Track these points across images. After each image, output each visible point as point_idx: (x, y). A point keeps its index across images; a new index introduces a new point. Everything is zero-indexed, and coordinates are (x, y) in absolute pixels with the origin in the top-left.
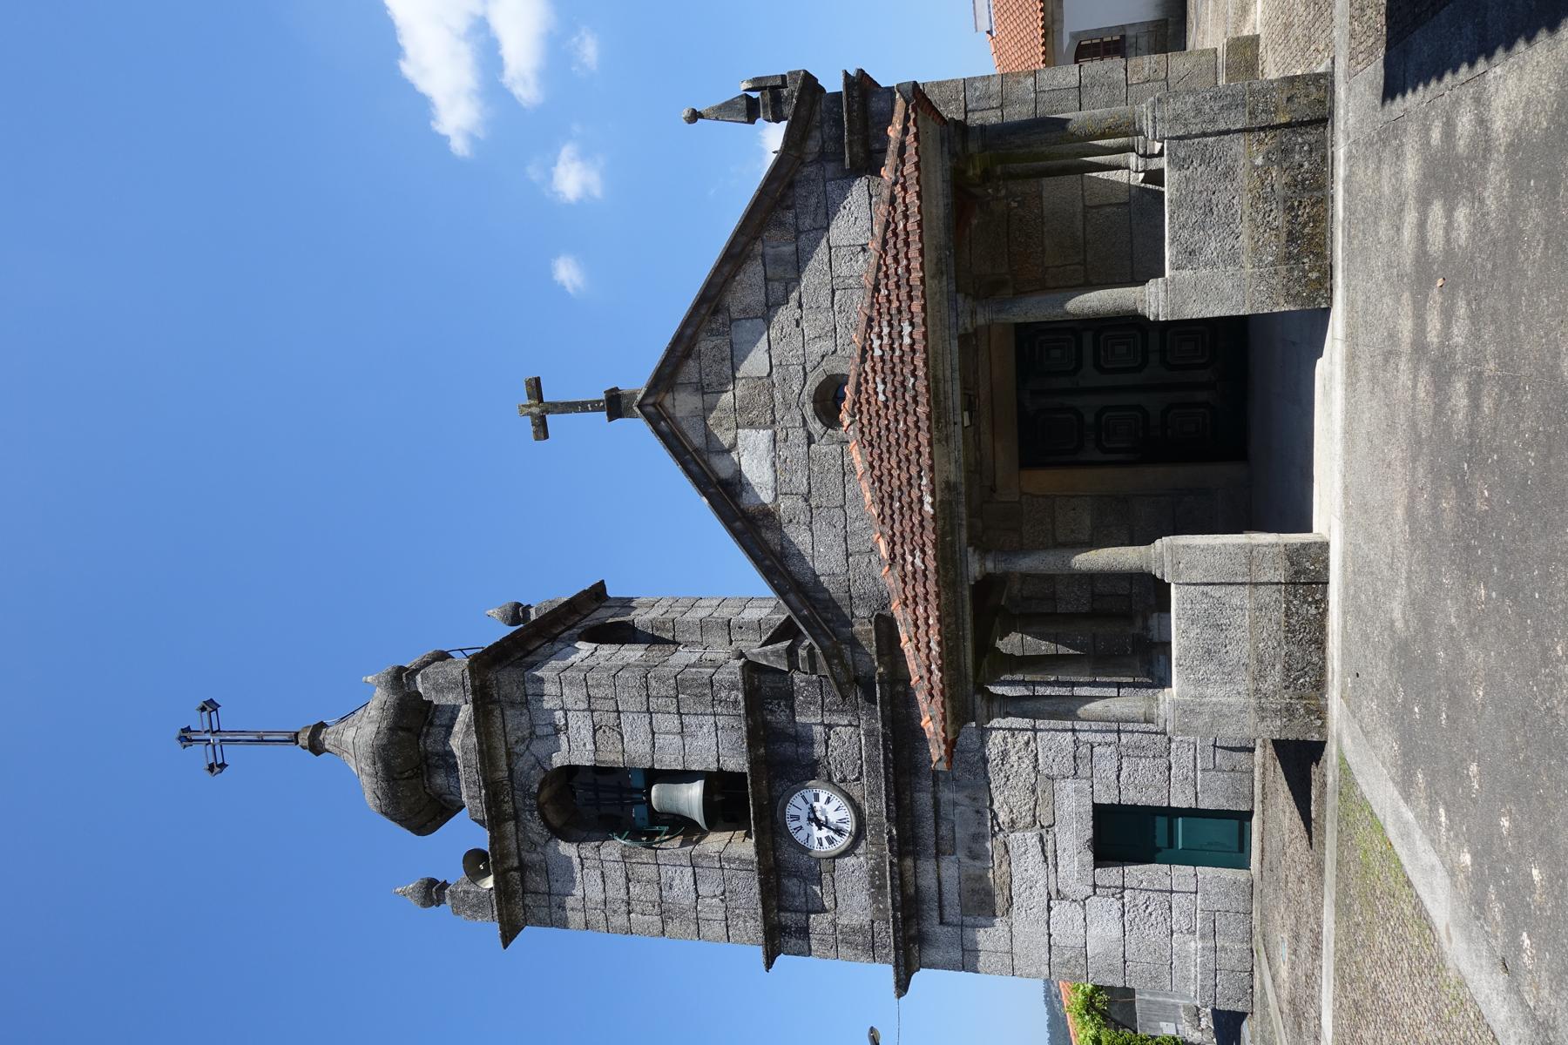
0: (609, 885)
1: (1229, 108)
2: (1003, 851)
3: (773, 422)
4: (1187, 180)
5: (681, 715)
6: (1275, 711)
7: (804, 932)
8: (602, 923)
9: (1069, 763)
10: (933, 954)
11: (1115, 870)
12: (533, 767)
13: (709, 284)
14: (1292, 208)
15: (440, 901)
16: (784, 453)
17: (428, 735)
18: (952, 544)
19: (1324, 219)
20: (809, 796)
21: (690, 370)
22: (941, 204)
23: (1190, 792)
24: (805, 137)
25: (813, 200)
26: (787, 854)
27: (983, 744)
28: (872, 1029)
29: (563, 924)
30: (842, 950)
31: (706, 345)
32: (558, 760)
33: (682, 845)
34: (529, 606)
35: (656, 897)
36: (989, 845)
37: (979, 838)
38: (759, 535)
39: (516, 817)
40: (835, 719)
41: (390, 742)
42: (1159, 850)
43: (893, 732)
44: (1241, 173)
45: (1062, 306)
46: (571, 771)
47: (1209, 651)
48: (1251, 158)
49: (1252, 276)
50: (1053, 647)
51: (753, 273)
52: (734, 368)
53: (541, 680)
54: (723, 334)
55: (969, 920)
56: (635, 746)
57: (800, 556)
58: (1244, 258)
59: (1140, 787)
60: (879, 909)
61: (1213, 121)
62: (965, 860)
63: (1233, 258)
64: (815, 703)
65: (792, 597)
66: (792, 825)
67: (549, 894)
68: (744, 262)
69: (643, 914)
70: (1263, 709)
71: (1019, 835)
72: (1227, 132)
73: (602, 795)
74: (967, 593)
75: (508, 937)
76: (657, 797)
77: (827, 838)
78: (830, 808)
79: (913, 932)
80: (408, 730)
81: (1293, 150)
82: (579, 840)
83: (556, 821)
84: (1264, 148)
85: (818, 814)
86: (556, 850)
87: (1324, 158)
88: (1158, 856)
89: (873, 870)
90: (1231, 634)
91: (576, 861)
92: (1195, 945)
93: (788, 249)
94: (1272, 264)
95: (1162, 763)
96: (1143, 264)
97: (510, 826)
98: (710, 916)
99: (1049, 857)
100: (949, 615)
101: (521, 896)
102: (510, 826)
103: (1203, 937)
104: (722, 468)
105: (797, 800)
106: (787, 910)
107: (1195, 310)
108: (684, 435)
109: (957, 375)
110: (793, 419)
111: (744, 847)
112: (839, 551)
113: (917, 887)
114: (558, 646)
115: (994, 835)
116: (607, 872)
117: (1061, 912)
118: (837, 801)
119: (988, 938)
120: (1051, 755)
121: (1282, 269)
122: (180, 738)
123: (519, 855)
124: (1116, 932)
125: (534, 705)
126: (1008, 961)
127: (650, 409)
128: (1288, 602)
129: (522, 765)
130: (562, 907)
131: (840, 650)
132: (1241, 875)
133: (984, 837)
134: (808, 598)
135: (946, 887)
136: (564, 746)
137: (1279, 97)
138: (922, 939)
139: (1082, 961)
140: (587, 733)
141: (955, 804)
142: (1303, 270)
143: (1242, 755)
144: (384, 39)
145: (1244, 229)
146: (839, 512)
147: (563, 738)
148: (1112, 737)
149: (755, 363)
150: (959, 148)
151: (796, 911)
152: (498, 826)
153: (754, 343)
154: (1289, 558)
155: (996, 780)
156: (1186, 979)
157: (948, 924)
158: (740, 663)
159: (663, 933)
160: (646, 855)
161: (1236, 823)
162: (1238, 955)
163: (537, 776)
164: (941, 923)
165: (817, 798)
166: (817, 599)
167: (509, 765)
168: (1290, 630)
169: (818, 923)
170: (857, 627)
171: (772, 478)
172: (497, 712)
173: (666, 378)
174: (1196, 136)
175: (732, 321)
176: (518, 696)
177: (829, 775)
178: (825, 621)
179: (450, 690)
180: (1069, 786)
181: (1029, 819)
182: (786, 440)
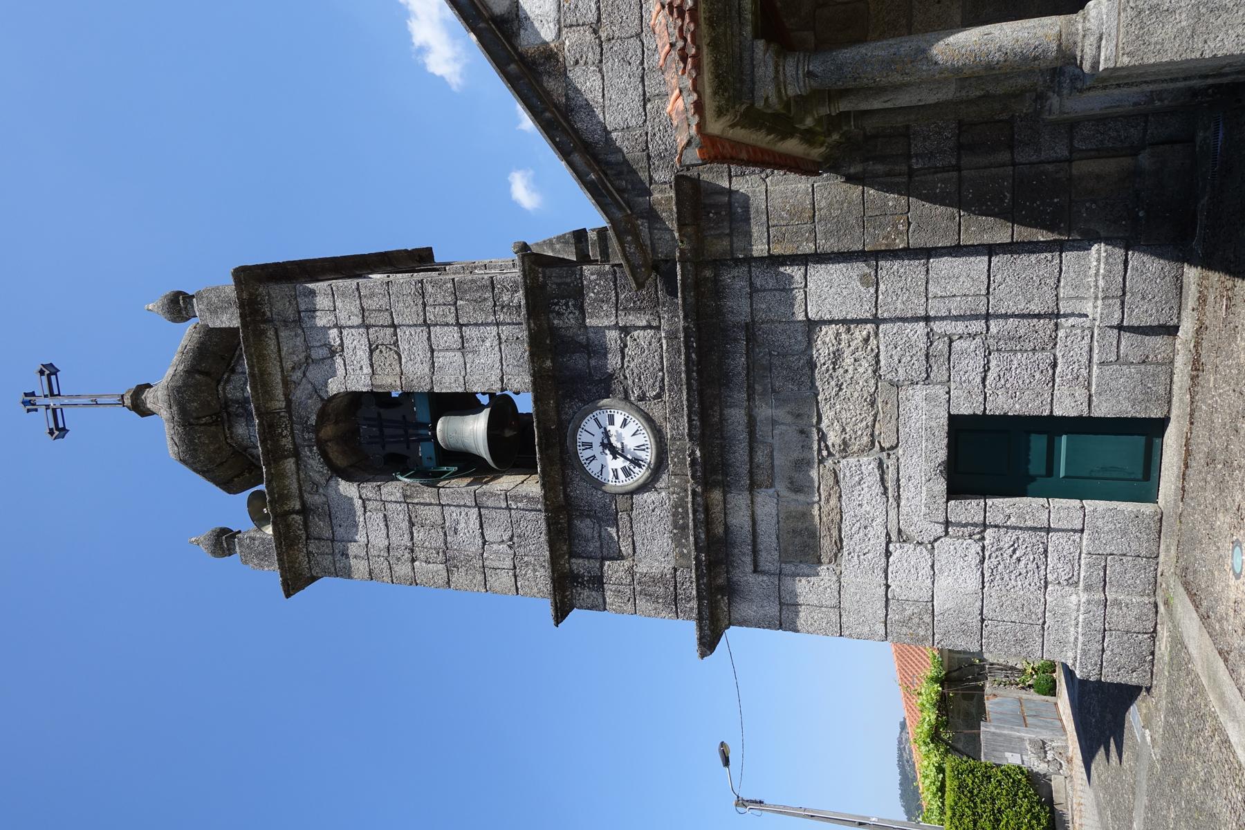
2: (831, 482)
5: (460, 326)
7: (598, 582)
8: (386, 572)
9: (920, 364)
10: (745, 609)
11: (974, 502)
15: (230, 552)
17: (228, 381)
23: (1081, 393)
26: (579, 490)
27: (810, 343)
28: (722, 744)
29: (347, 573)
30: (641, 603)
32: (334, 387)
35: (440, 543)
36: (814, 474)
37: (802, 465)
39: (296, 454)
40: (631, 319)
41: (185, 384)
42: (1033, 479)
43: (699, 329)
46: (355, 399)
55: (789, 568)
57: (588, 108)
59: (1010, 391)
60: (682, 555)
62: (784, 493)
64: (607, 302)
65: (576, 157)
66: (584, 454)
69: (428, 562)
71: (852, 460)
73: (387, 431)
76: (443, 431)
77: (624, 469)
78: (627, 433)
79: (721, 581)
80: (206, 374)
83: (340, 461)
85: (613, 440)
86: (337, 490)
88: (1031, 487)
89: (676, 507)
91: (358, 503)
92: (1077, 598)
95: (1045, 357)
97: (290, 464)
98: (496, 564)
99: (891, 490)
102: (290, 464)
103: (1088, 588)
105: (589, 424)
106: (580, 556)
111: (532, 486)
112: (635, 96)
113: (727, 527)
115: (821, 462)
116: (388, 513)
117: (905, 560)
118: (635, 423)
119: (809, 590)
120: (896, 354)
122: (24, 403)
123: (301, 497)
124: (973, 583)
125: (307, 323)
126: (834, 618)
129: (299, 394)
131: (635, 227)
132: (1147, 508)
133: (809, 464)
134: (598, 162)
135: (762, 527)
136: (341, 371)
138: (731, 590)
139: (927, 619)
140: (363, 354)
141: (774, 422)
143: (1158, 341)
144: (404, 14)
146: (635, 42)
147: (339, 360)
148: (978, 326)
151: (589, 558)
155: (825, 390)
156: (1062, 643)
157: (764, 573)
160: (428, 494)
161: (1140, 440)
162: (1136, 611)
163: (314, 406)
164: (755, 571)
165: (612, 422)
166: (608, 163)
167: (286, 396)
169: (614, 571)
170: (657, 195)
172: (271, 333)
176: (290, 313)
177: (626, 392)
178: (618, 190)
179: (224, 309)
180: (918, 394)
181: (866, 439)
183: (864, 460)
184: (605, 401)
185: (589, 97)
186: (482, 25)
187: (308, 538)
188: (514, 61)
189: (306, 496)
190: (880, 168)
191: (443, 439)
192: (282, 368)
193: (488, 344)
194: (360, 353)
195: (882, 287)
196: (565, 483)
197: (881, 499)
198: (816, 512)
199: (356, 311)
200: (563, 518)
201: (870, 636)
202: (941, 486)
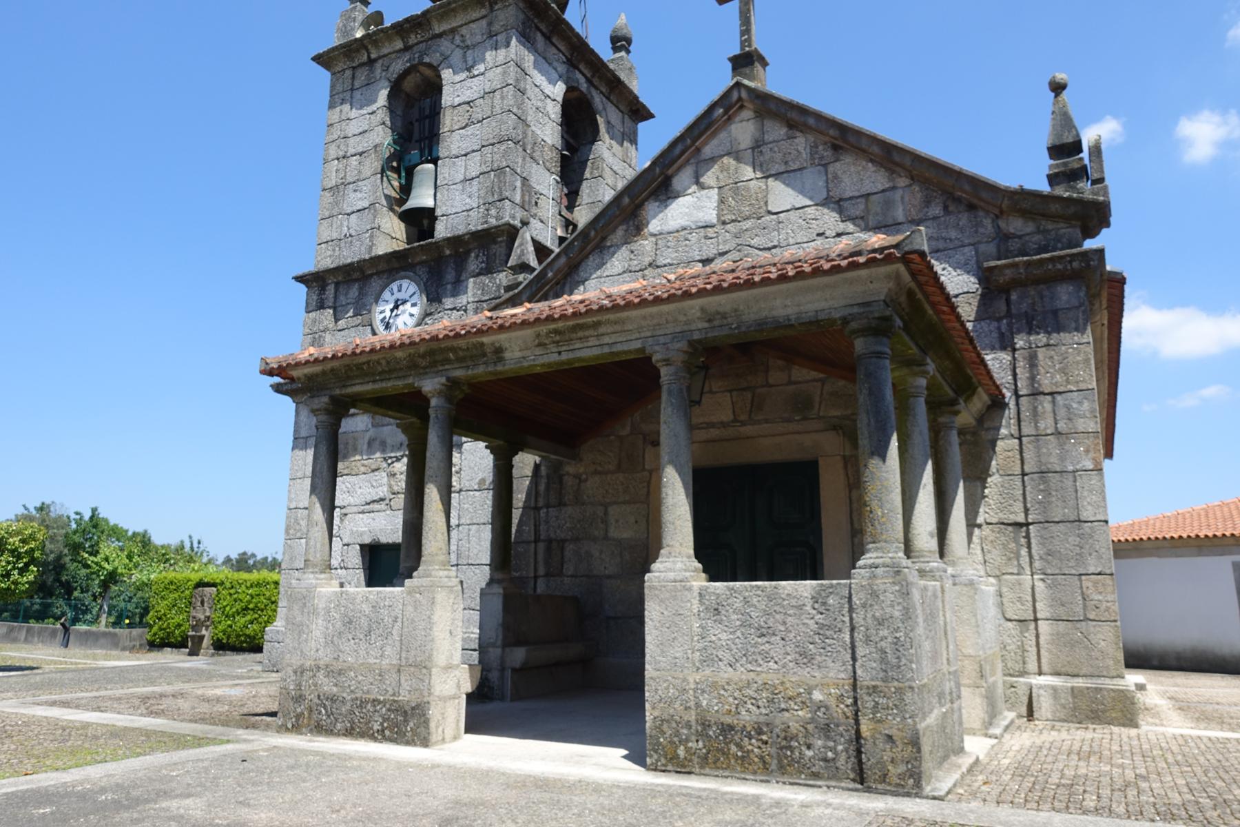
0: (358, 139)
1: (883, 660)
2: (374, 467)
3: (724, 223)
4: (800, 607)
6: (300, 685)
7: (321, 306)
12: (442, 55)
13: (859, 133)
14: (760, 732)
16: (694, 237)
18: (448, 361)
19: (745, 770)
20: (415, 299)
21: (776, 131)
22: (789, 311)
24: (1026, 214)
25: (953, 234)
26: (375, 283)
31: (801, 143)
33: (386, 196)
34: (628, 52)
35: (349, 179)
36: (378, 455)
38: (621, 223)
39: (407, 48)
44: (804, 673)
45: (671, 462)
47: (350, 622)
48: (823, 686)
49: (685, 680)
50: (521, 505)
51: (872, 179)
52: (777, 176)
53: (508, 45)
54: (812, 158)
56: (456, 138)
57: (601, 265)
58: (708, 672)
61: (868, 640)
63: (709, 660)
64: (482, 294)
66: (394, 286)
67: (352, 90)
68: (887, 169)
69: (337, 171)
70: (302, 673)
71: (386, 479)
72: (854, 659)
74: (410, 380)
75: (321, 59)
81: (828, 738)
82: (391, 108)
84: (832, 702)
87: (816, 776)
90: (363, 645)
91: (374, 107)
93: (900, 215)
94: (698, 705)
96: (720, 556)
100: (388, 363)
101: (347, 62)
102: (399, 45)
104: (682, 179)
106: (336, 290)
107: (653, 613)
108: (714, 135)
109: (606, 350)
110: (725, 242)
114: (562, 68)
121: (692, 716)
125: (488, 43)
127: (735, 96)
128: (384, 703)
130: (343, 102)
133: (383, 451)
137: (893, 725)
139: (299, 535)
142: (687, 740)
145: (740, 674)
147: (464, 75)
149: (782, 196)
150: (854, 325)
151: (336, 297)
152: (397, 33)
153: (802, 192)
154: (418, 706)
158: (517, 223)
159: (324, 190)
165: (414, 305)
166: (564, 284)
168: (362, 703)
171: (671, 228)
172: (484, 12)
173: (770, 108)
174: (851, 619)
175: (825, 166)
177: (431, 314)
182: (706, 238)
183: (385, 489)
184: (425, 299)
185: (608, 265)
186: (658, 170)
187: (354, 68)
188: (632, 201)
189: (380, 61)
190: (542, 487)
191: (422, 169)
192: (461, 26)
193: (468, 200)
194: (468, 93)
195: (477, 494)
196: (378, 273)
197: (363, 501)
198: (358, 457)
199: (494, 87)
200: (356, 275)
201: (290, 500)
202: (367, 540)
